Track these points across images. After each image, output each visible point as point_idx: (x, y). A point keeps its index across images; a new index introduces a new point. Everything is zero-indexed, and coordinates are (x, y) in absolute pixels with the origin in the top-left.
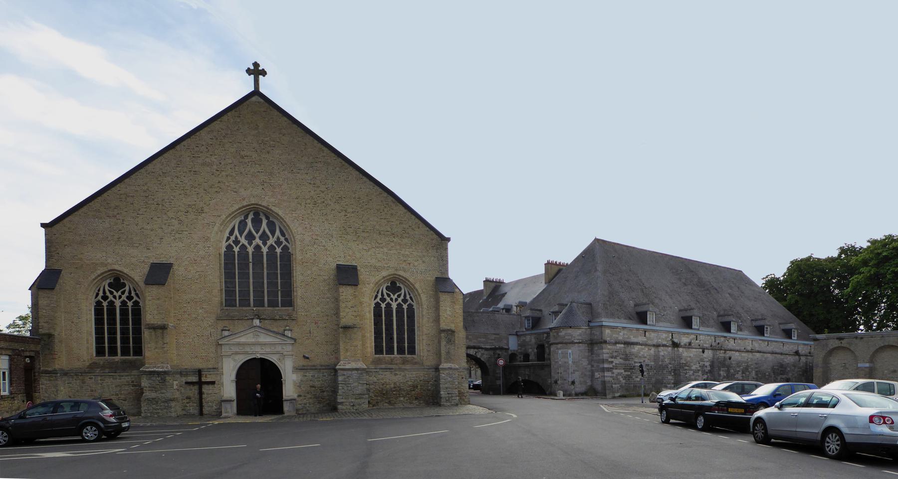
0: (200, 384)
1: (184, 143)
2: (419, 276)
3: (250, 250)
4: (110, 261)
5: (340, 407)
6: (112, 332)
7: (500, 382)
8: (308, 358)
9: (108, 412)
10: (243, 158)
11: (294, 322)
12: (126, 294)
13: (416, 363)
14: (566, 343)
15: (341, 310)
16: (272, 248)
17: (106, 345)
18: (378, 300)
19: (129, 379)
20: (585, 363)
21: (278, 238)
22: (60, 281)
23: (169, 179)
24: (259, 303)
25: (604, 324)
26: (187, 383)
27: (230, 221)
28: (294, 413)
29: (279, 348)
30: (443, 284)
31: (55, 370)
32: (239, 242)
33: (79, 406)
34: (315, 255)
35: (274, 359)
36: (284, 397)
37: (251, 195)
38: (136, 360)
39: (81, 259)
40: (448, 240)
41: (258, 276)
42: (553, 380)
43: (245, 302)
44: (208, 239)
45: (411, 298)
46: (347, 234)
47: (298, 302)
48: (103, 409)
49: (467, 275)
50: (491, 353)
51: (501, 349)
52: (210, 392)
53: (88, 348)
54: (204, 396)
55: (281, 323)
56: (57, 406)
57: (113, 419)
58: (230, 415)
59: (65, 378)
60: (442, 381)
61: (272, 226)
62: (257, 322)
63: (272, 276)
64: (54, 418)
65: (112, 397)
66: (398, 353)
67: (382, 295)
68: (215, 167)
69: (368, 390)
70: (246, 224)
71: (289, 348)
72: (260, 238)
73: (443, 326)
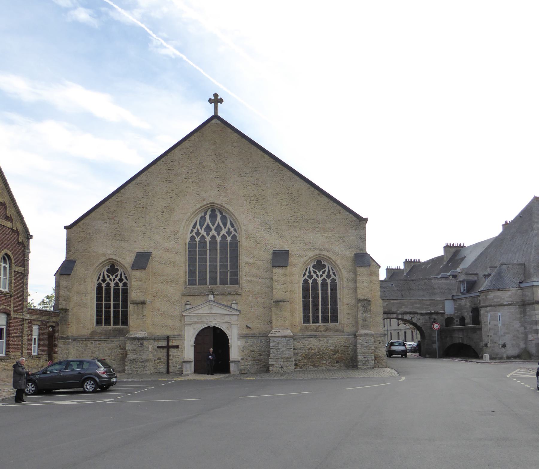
0: (168, 347)
1: (163, 159)
2: (340, 256)
3: (208, 239)
4: (108, 252)
5: (271, 368)
6: (108, 307)
7: (436, 346)
8: (250, 328)
9: (102, 370)
10: (204, 167)
11: (239, 297)
12: (119, 277)
13: (337, 330)
14: (495, 306)
15: (274, 287)
16: (224, 237)
17: (103, 317)
18: (306, 277)
19: (117, 343)
20: (517, 325)
21: (229, 229)
22: (75, 268)
23: (151, 187)
24: (213, 282)
25: (535, 284)
26: (158, 347)
27: (194, 217)
28: (238, 373)
29: (227, 319)
30: (363, 260)
31: (68, 337)
32: (200, 233)
33: (83, 364)
34: (257, 241)
35: (223, 327)
36: (231, 359)
37: (210, 195)
38: (123, 329)
39: (89, 252)
40: (366, 220)
41: (213, 260)
42: (484, 343)
43: (203, 282)
44: (177, 232)
45: (334, 273)
46: (282, 225)
47: (243, 280)
48: (99, 367)
49: (390, 248)
50: (427, 317)
51: (437, 313)
52: (175, 354)
53: (91, 320)
54: (171, 358)
55: (230, 298)
56: (68, 364)
57: (105, 376)
58: (189, 373)
59: (74, 343)
60: (359, 346)
61: (224, 219)
62: (211, 297)
63: (224, 259)
64: (66, 374)
65: (105, 358)
66: (323, 321)
67: (310, 272)
68: (184, 176)
69: (295, 354)
70: (205, 218)
71: (235, 318)
72: (216, 229)
73: (360, 296)
